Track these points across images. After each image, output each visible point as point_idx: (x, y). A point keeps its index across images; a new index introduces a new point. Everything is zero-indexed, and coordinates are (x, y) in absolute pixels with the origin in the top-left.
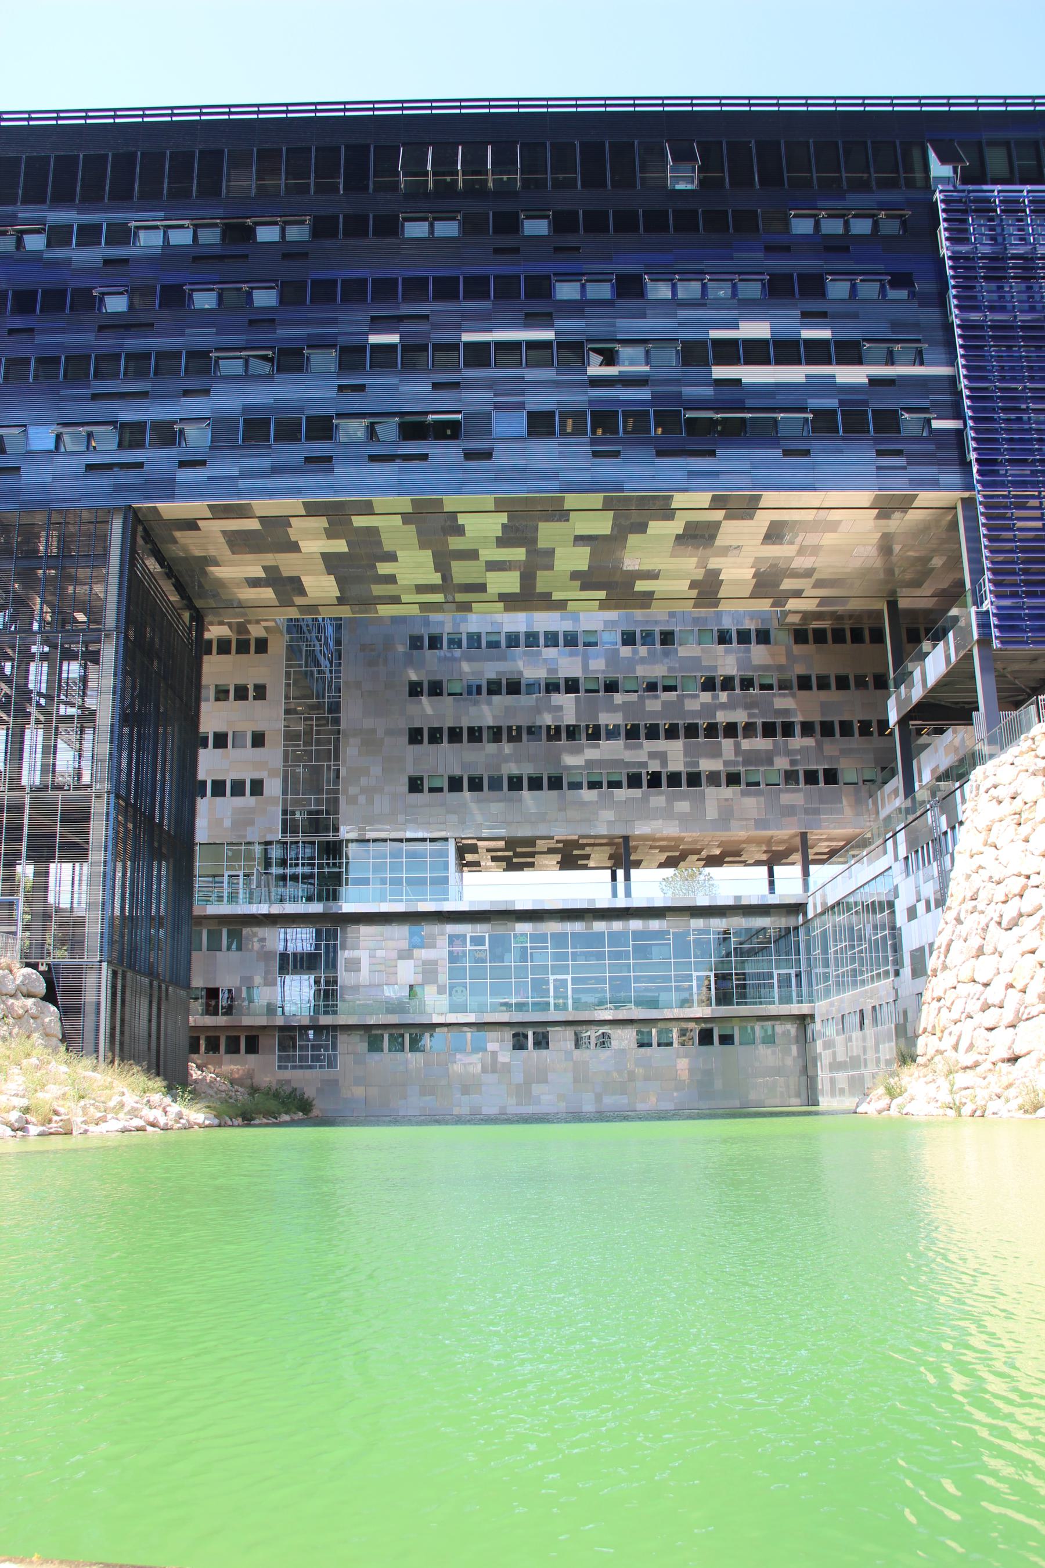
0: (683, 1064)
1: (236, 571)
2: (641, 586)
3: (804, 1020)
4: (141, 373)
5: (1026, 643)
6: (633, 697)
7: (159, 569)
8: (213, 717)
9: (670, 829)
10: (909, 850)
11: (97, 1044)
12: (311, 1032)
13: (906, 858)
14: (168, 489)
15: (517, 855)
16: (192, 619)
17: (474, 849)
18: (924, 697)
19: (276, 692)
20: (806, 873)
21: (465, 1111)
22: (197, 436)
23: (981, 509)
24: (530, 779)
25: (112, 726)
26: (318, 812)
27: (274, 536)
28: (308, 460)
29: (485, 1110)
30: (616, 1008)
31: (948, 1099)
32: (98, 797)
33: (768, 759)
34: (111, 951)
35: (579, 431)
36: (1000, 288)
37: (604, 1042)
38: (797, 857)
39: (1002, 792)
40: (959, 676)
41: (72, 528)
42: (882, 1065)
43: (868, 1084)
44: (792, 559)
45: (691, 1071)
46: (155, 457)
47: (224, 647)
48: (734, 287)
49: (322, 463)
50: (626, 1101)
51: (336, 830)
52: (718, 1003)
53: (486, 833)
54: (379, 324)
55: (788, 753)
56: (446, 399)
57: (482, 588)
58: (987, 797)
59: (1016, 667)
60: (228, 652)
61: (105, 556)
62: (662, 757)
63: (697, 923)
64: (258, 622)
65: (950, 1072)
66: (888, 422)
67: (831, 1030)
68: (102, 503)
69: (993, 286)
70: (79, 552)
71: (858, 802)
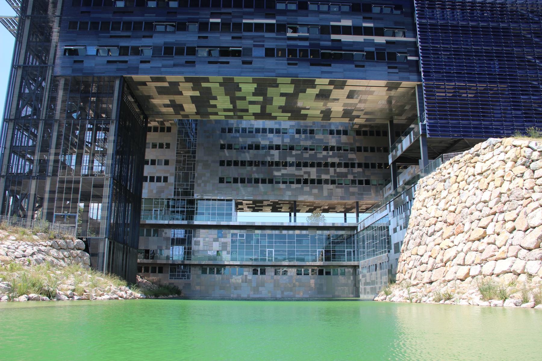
0: (312, 281)
1: (160, 101)
2: (303, 112)
3: (355, 267)
5: (438, 136)
6: (299, 152)
7: (133, 100)
8: (150, 154)
9: (310, 199)
10: (395, 208)
11: (103, 268)
12: (182, 267)
13: (394, 211)
14: (136, 70)
15: (256, 206)
16: (144, 118)
17: (241, 204)
18: (402, 155)
19: (174, 146)
20: (358, 216)
21: (235, 296)
22: (148, 53)
23: (424, 88)
24: (262, 180)
25: (113, 154)
26: (187, 189)
27: (173, 89)
28: (187, 62)
29: (242, 296)
30: (290, 261)
31: (408, 296)
32: (107, 179)
33: (345, 175)
34: (109, 234)
35: (283, 55)
36: (433, 12)
37: (285, 273)
38: (355, 210)
39: (429, 188)
40: (414, 147)
41: (102, 83)
42: (383, 283)
43: (378, 290)
44: (357, 104)
45: (315, 284)
46: (132, 59)
47: (156, 129)
48: (340, 7)
49: (192, 63)
50: (292, 294)
51: (193, 195)
52: (326, 261)
53: (246, 198)
54: (213, 15)
55: (353, 173)
56: (237, 43)
57: (247, 111)
58: (423, 189)
59: (434, 145)
60: (157, 131)
61: (113, 93)
62: (309, 173)
63: (319, 232)
64: (168, 121)
65: (408, 287)
66: (392, 57)
67: (365, 271)
68: (112, 75)
69: (430, 10)
70: (105, 91)
71: (377, 192)
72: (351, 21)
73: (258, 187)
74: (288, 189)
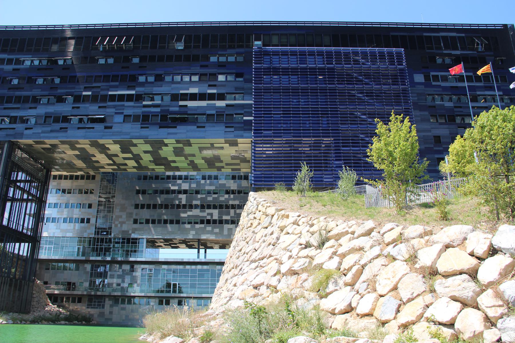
2: (173, 165)
4: (19, 102)
6: (204, 196)
15: (170, 243)
19: (97, 191)
22: (33, 121)
28: (61, 128)
46: (19, 127)
54: (86, 89)
60: (84, 179)
62: (211, 215)
72: (197, 89)
73: (167, 227)
74: (193, 228)
